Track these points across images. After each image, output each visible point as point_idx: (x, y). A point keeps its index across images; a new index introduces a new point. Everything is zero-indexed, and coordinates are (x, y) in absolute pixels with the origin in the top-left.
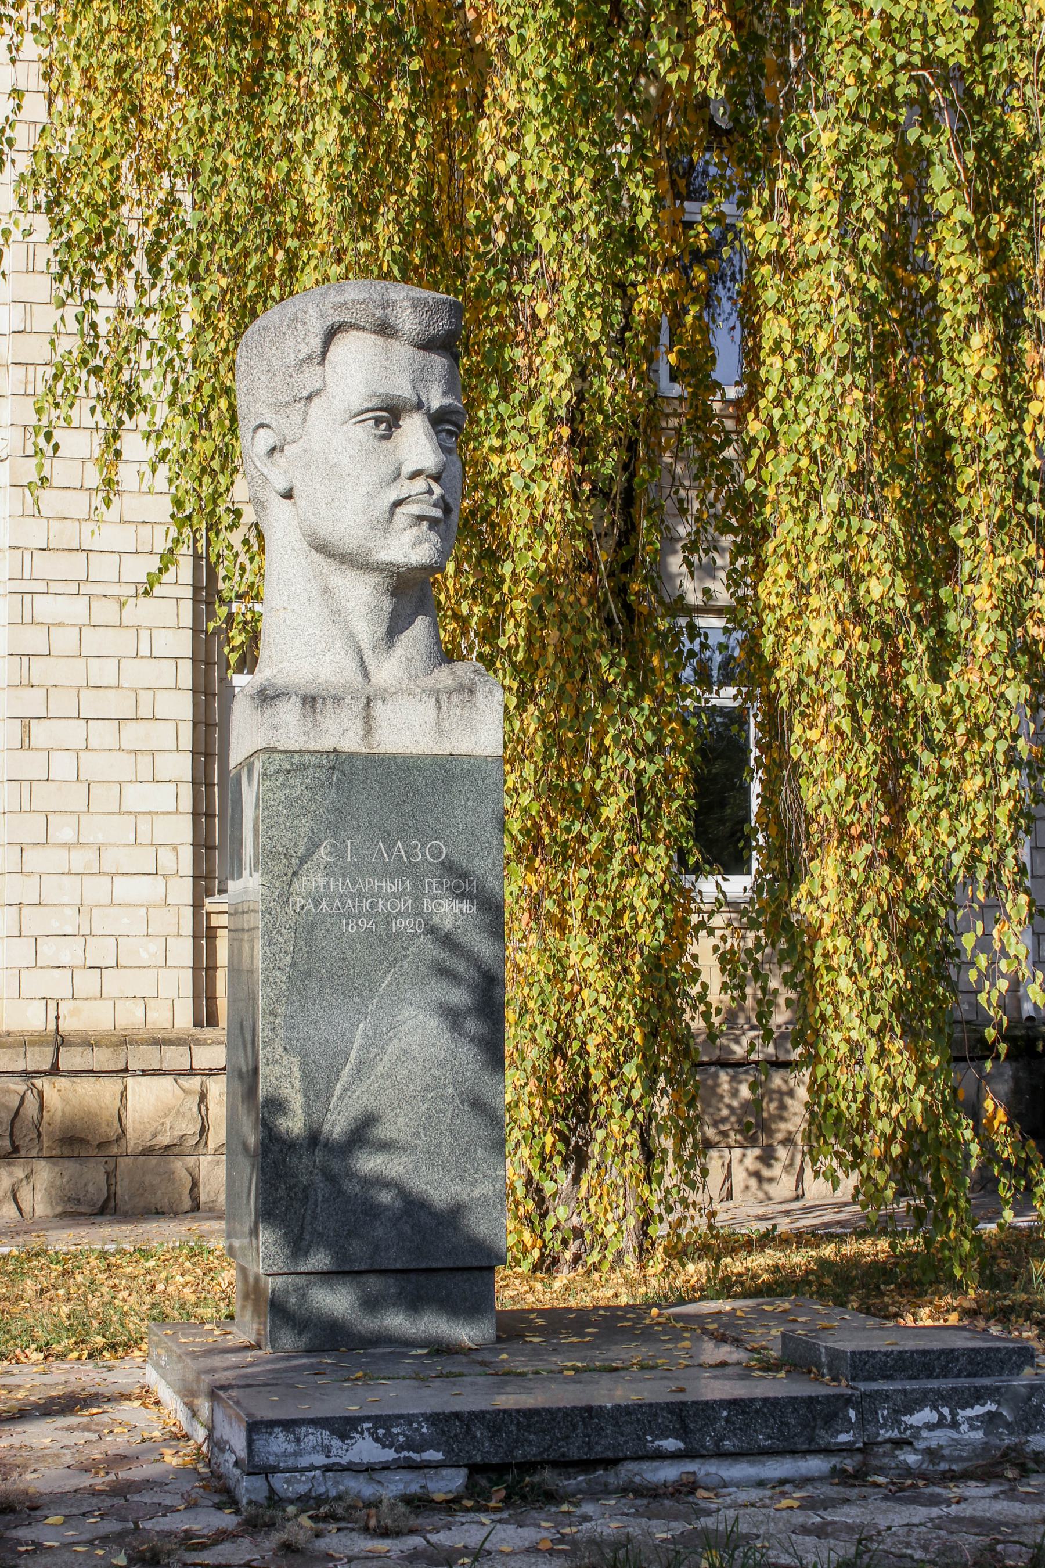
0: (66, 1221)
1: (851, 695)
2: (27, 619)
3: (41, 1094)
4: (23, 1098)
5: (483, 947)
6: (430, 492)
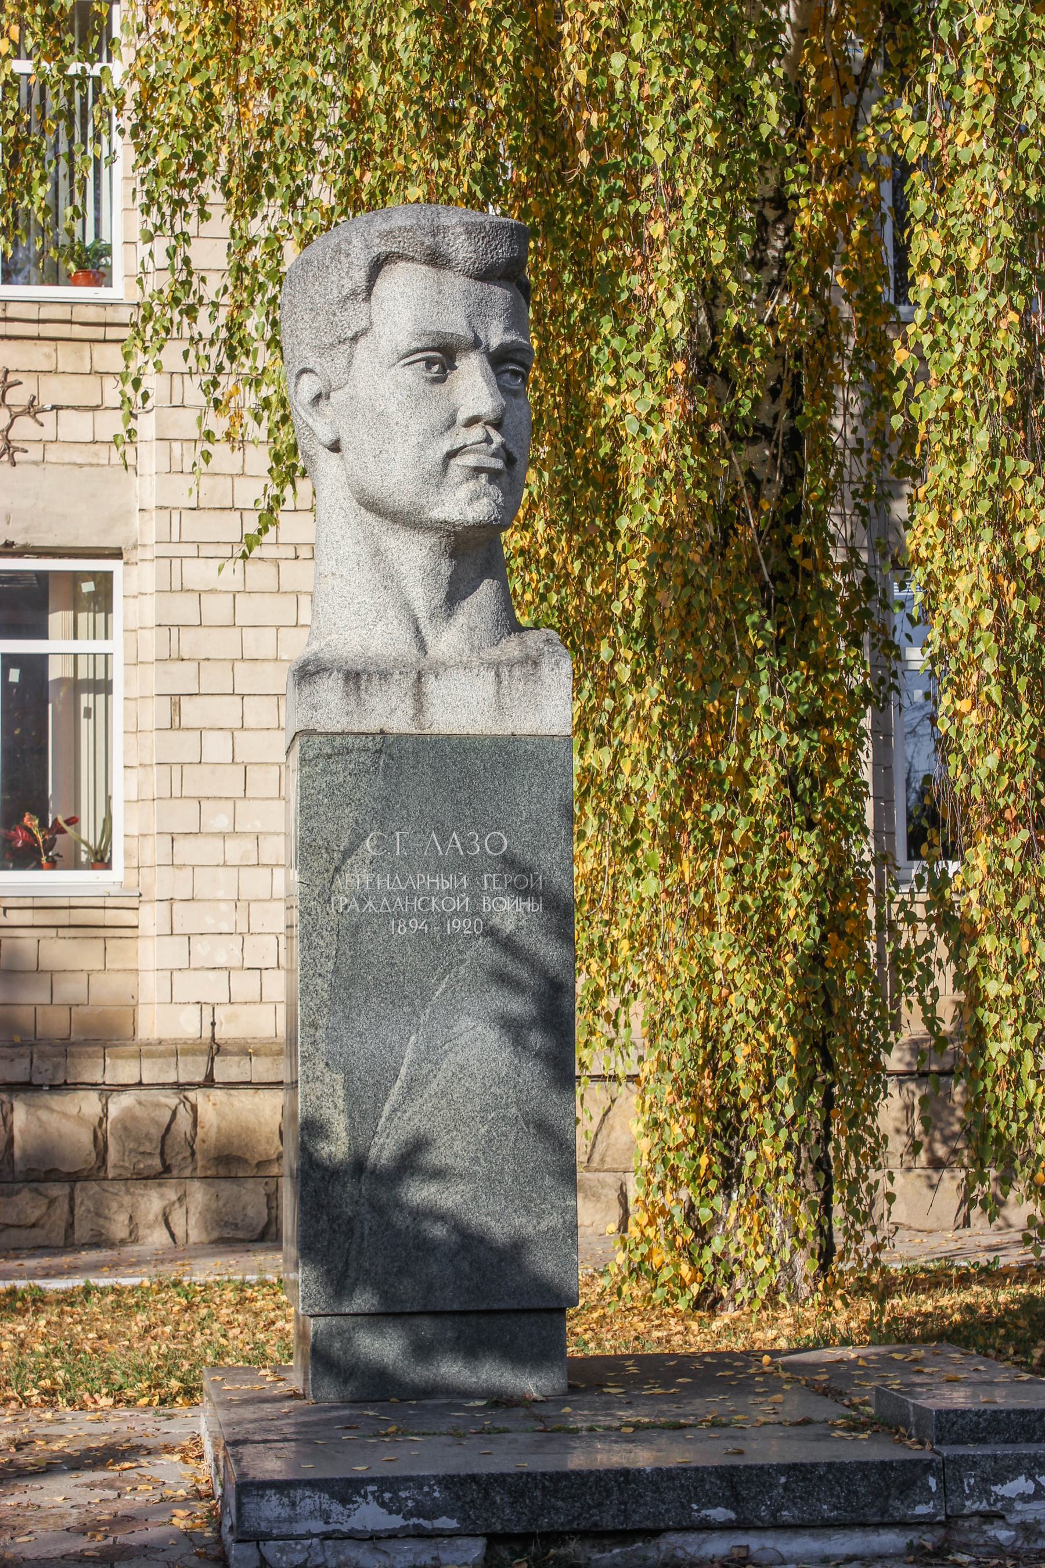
0: (222, 1248)
1: (1004, 659)
2: (176, 586)
3: (194, 1108)
4: (174, 1113)
5: (550, 952)
6: (488, 440)
